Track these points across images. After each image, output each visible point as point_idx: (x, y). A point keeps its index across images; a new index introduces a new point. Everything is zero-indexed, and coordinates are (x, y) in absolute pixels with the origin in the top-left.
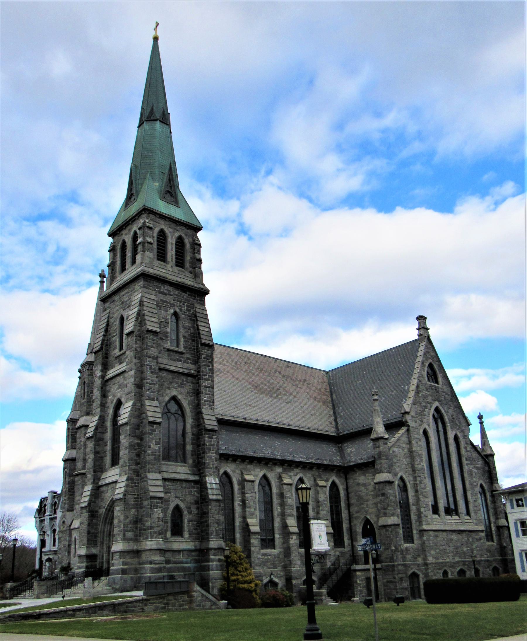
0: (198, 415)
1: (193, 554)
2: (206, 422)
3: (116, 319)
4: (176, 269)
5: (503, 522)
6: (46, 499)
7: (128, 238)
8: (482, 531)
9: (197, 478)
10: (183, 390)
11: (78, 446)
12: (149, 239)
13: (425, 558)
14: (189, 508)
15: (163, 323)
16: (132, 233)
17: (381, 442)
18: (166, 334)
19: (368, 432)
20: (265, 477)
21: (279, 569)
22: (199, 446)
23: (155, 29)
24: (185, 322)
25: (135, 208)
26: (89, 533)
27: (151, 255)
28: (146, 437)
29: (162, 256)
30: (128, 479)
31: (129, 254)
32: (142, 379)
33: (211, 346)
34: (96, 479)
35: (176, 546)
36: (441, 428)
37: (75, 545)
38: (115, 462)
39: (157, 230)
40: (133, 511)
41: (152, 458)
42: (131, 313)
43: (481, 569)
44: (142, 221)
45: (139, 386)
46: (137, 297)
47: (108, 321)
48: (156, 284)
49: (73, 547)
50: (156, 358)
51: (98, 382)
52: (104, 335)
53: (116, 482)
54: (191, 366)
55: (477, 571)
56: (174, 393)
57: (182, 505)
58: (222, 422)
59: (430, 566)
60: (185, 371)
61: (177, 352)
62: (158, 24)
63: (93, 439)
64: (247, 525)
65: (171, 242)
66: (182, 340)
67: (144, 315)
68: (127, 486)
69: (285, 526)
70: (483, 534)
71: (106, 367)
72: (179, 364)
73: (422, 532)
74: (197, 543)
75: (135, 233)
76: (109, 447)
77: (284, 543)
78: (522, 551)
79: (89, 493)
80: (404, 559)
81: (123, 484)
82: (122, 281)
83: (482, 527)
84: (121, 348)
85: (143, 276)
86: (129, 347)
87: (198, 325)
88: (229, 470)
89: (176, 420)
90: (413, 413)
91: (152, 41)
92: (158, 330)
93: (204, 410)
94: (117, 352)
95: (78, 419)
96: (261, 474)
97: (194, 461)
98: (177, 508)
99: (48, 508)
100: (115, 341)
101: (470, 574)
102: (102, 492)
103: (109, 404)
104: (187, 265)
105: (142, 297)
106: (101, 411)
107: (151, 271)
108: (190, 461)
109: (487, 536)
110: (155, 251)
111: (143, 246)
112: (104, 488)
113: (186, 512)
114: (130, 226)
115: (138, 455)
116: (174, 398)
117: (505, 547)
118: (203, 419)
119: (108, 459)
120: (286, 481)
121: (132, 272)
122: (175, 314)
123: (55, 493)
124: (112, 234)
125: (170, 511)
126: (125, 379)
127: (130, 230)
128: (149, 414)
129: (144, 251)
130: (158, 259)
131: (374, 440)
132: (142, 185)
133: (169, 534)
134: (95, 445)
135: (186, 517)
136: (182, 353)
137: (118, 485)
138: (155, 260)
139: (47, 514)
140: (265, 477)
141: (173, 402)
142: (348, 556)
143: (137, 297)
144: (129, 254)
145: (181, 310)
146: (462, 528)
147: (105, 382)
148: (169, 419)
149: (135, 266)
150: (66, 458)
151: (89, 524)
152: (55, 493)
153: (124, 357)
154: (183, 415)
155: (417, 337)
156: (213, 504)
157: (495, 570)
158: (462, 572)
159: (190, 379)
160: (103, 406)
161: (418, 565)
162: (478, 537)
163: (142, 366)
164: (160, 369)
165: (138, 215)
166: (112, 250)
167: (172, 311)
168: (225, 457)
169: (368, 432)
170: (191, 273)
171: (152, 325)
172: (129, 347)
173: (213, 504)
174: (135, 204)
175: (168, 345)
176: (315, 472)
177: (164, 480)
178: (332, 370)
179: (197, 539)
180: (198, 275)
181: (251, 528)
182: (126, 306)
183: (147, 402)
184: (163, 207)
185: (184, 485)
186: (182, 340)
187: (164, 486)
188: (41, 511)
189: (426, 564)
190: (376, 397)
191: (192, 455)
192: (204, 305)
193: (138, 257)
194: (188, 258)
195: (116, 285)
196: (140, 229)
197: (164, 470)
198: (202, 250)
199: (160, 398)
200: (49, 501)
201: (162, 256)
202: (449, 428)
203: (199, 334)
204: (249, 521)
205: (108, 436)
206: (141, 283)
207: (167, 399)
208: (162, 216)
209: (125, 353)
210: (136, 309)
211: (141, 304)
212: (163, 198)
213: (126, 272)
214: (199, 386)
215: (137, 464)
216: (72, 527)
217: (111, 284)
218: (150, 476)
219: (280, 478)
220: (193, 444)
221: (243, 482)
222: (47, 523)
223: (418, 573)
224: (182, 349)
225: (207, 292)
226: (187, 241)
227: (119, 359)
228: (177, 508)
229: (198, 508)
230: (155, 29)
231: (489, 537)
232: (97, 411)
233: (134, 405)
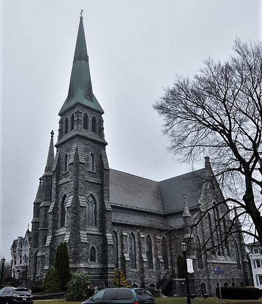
0: (102, 204)
3: (63, 156)
4: (92, 133)
5: (246, 260)
6: (17, 240)
7: (69, 118)
8: (236, 264)
9: (102, 234)
10: (95, 191)
11: (40, 216)
13: (208, 276)
15: (87, 159)
18: (88, 164)
23: (81, 13)
24: (96, 158)
25: (72, 103)
26: (50, 258)
27: (81, 126)
29: (86, 127)
31: (69, 125)
32: (77, 186)
33: (108, 170)
34: (53, 233)
37: (39, 264)
38: (63, 225)
41: (82, 224)
42: (71, 154)
45: (76, 189)
48: (83, 140)
49: (37, 265)
50: (84, 176)
51: (54, 186)
54: (99, 180)
58: (112, 206)
60: (97, 182)
62: (82, 11)
63: (52, 214)
65: (90, 119)
66: (95, 167)
67: (78, 155)
69: (141, 258)
70: (236, 266)
72: (93, 178)
73: (207, 264)
74: (102, 265)
76: (60, 218)
77: (141, 266)
78: (257, 275)
80: (199, 276)
82: (66, 138)
84: (66, 171)
85: (77, 136)
86: (71, 170)
94: (64, 172)
95: (40, 203)
97: (100, 225)
99: (18, 245)
100: (63, 167)
101: (230, 285)
102: (56, 240)
105: (77, 146)
109: (238, 266)
111: (78, 122)
116: (91, 195)
119: (59, 224)
121: (71, 134)
122: (92, 154)
123: (21, 238)
128: (81, 202)
132: (76, 91)
134: (53, 217)
136: (95, 173)
144: (69, 125)
147: (58, 186)
149: (73, 131)
154: (95, 203)
156: (110, 246)
157: (242, 283)
158: (226, 284)
159: (99, 186)
160: (57, 198)
162: (234, 267)
163: (77, 179)
165: (75, 106)
166: (61, 122)
168: (114, 224)
169: (182, 212)
170: (99, 134)
172: (71, 170)
173: (110, 246)
177: (87, 234)
179: (102, 263)
180: (102, 135)
182: (69, 150)
183: (79, 197)
184: (86, 103)
188: (14, 246)
189: (209, 279)
190: (185, 196)
193: (75, 127)
194: (97, 127)
195: (63, 140)
196: (75, 113)
197: (87, 229)
200: (18, 242)
201: (86, 127)
207: (88, 195)
210: (74, 152)
211: (77, 149)
212: (86, 98)
213: (68, 133)
216: (37, 255)
217: (60, 139)
218: (81, 232)
219: (139, 234)
221: (122, 236)
222: (17, 252)
225: (107, 144)
226: (97, 119)
227: (65, 175)
230: (81, 13)
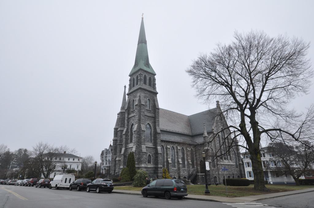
0: (155, 129)
1: (154, 168)
2: (157, 131)
4: (149, 87)
5: (241, 162)
6: (104, 151)
7: (135, 78)
8: (235, 165)
9: (155, 147)
10: (151, 121)
11: (118, 136)
12: (142, 78)
13: (218, 172)
14: (152, 155)
15: (146, 102)
16: (136, 76)
17: (206, 138)
19: (202, 134)
20: (173, 147)
21: (177, 174)
22: (155, 138)
23: (142, 15)
25: (137, 69)
26: (124, 162)
27: (142, 82)
28: (142, 135)
29: (145, 83)
30: (136, 147)
31: (135, 82)
32: (140, 118)
33: (158, 109)
34: (126, 146)
35: (149, 166)
36: (223, 134)
38: (131, 142)
39: (144, 75)
40: (137, 156)
41: (143, 141)
42: (137, 99)
43: (234, 176)
44: (140, 73)
45: (139, 120)
46: (138, 95)
47: (129, 101)
48: (144, 91)
49: (116, 165)
51: (126, 118)
52: (128, 105)
53: (132, 147)
54: (153, 115)
55: (233, 177)
56: (148, 122)
57: (151, 154)
58: (161, 131)
59: (220, 175)
60: (152, 116)
61: (149, 110)
62: (143, 14)
64: (168, 161)
65: (148, 78)
66: (151, 107)
68: (136, 149)
69: (178, 161)
70: (235, 166)
71: (129, 114)
72: (150, 114)
74: (155, 166)
75: (137, 76)
76: (129, 137)
77: (178, 166)
78: (248, 171)
79: (124, 150)
81: (135, 148)
83: (234, 164)
84: (133, 109)
85: (140, 88)
87: (155, 103)
88: (163, 145)
89: (149, 130)
90: (215, 129)
91: (141, 19)
92: (144, 104)
93: (157, 128)
94: (132, 110)
95: (118, 128)
96: (172, 146)
98: (149, 155)
99: (104, 154)
101: (231, 178)
102: (127, 150)
103: (129, 125)
104: (152, 85)
105: (140, 94)
106: (127, 127)
107: (142, 87)
108: (153, 142)
109: (236, 166)
110: (143, 81)
112: (128, 149)
113: (152, 157)
114: (136, 74)
115: (139, 140)
116: (148, 124)
117: (241, 170)
118: (157, 130)
119: (129, 141)
120: (179, 148)
121: (136, 87)
122: (149, 99)
124: (130, 76)
125: (147, 156)
126: (134, 118)
127: (136, 75)
128: (142, 128)
129: (140, 81)
130: (144, 84)
131: (204, 137)
133: (147, 163)
134: (126, 137)
135: (152, 158)
136: (151, 111)
137: (133, 148)
138: (143, 84)
139: (104, 155)
140: (173, 147)
141: (148, 125)
142: (196, 171)
143: (138, 95)
144: (135, 82)
145: (150, 98)
146: (229, 164)
147: (129, 119)
148: (147, 129)
149: (137, 85)
150: (114, 139)
151: (124, 159)
152: (107, 149)
153: (135, 111)
154: (151, 128)
155: (216, 107)
158: (229, 177)
159: (153, 118)
160: (128, 125)
161: (216, 174)
162: (234, 167)
164: (145, 115)
166: (130, 80)
167: (148, 99)
168: (162, 141)
169: (202, 134)
171: (143, 103)
172: (136, 109)
173: (160, 154)
174: (137, 67)
175: (147, 109)
176: (186, 146)
177: (146, 147)
178: (190, 116)
180: (154, 88)
181: (169, 162)
182: (135, 97)
183: (141, 125)
184: (145, 68)
185: (151, 149)
186: (151, 107)
187: (146, 149)
188: (102, 154)
189: (219, 174)
190: (205, 125)
191: (153, 140)
192: (156, 97)
193: (139, 83)
194: (152, 83)
195: (132, 91)
196: (139, 75)
198: (156, 81)
199: (145, 124)
200: (105, 152)
201: (145, 83)
202: (225, 134)
203: (155, 105)
204: (169, 159)
205: (129, 134)
206: (140, 90)
207: (147, 124)
208: (145, 71)
209: (135, 110)
210: (138, 98)
211: (140, 96)
212: (145, 66)
213: (134, 87)
214: (155, 120)
215: (139, 142)
218: (142, 146)
219: (177, 147)
220: (153, 137)
221: (167, 148)
222: (104, 158)
223: (217, 177)
224: (150, 110)
227: (133, 112)
228: (149, 155)
229: (155, 156)
230: (142, 15)
231: (237, 167)
232: (126, 126)
233: (138, 126)
